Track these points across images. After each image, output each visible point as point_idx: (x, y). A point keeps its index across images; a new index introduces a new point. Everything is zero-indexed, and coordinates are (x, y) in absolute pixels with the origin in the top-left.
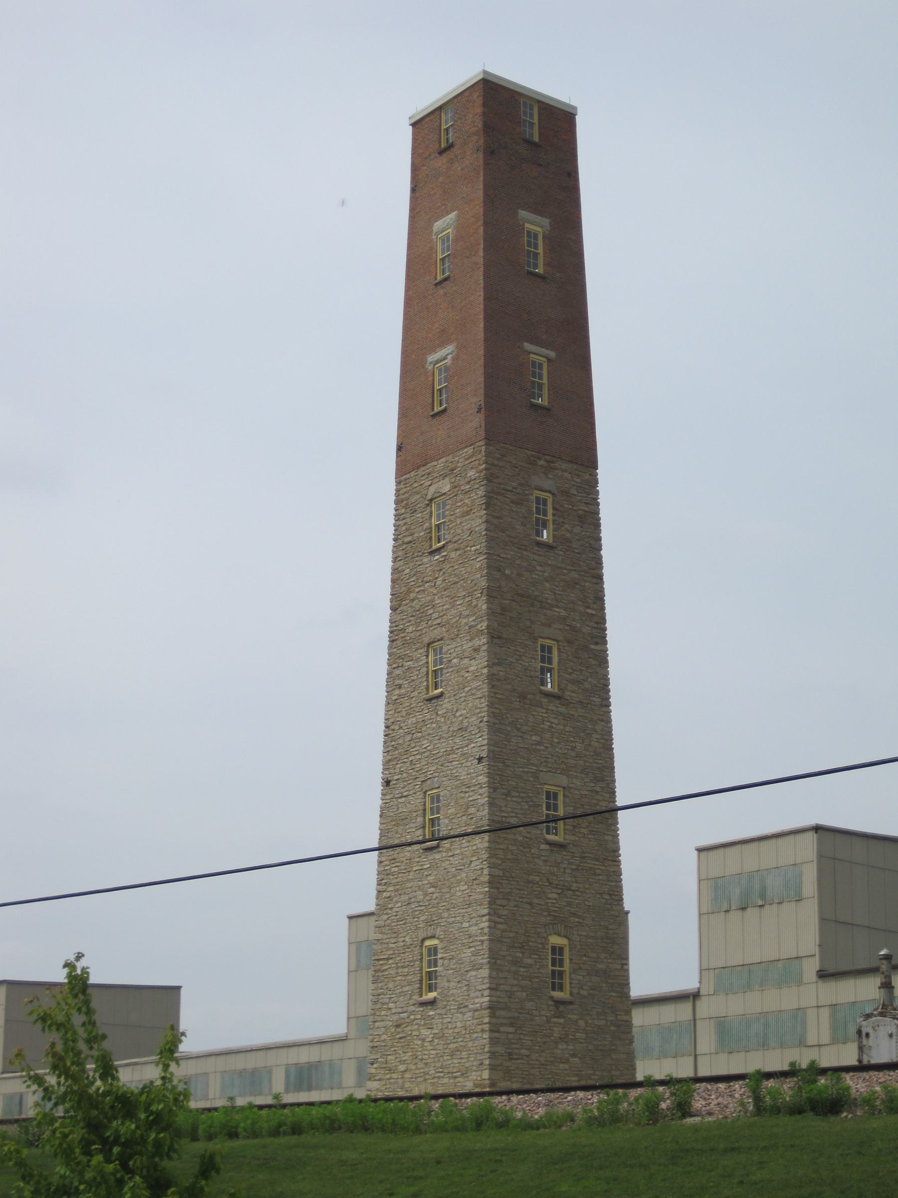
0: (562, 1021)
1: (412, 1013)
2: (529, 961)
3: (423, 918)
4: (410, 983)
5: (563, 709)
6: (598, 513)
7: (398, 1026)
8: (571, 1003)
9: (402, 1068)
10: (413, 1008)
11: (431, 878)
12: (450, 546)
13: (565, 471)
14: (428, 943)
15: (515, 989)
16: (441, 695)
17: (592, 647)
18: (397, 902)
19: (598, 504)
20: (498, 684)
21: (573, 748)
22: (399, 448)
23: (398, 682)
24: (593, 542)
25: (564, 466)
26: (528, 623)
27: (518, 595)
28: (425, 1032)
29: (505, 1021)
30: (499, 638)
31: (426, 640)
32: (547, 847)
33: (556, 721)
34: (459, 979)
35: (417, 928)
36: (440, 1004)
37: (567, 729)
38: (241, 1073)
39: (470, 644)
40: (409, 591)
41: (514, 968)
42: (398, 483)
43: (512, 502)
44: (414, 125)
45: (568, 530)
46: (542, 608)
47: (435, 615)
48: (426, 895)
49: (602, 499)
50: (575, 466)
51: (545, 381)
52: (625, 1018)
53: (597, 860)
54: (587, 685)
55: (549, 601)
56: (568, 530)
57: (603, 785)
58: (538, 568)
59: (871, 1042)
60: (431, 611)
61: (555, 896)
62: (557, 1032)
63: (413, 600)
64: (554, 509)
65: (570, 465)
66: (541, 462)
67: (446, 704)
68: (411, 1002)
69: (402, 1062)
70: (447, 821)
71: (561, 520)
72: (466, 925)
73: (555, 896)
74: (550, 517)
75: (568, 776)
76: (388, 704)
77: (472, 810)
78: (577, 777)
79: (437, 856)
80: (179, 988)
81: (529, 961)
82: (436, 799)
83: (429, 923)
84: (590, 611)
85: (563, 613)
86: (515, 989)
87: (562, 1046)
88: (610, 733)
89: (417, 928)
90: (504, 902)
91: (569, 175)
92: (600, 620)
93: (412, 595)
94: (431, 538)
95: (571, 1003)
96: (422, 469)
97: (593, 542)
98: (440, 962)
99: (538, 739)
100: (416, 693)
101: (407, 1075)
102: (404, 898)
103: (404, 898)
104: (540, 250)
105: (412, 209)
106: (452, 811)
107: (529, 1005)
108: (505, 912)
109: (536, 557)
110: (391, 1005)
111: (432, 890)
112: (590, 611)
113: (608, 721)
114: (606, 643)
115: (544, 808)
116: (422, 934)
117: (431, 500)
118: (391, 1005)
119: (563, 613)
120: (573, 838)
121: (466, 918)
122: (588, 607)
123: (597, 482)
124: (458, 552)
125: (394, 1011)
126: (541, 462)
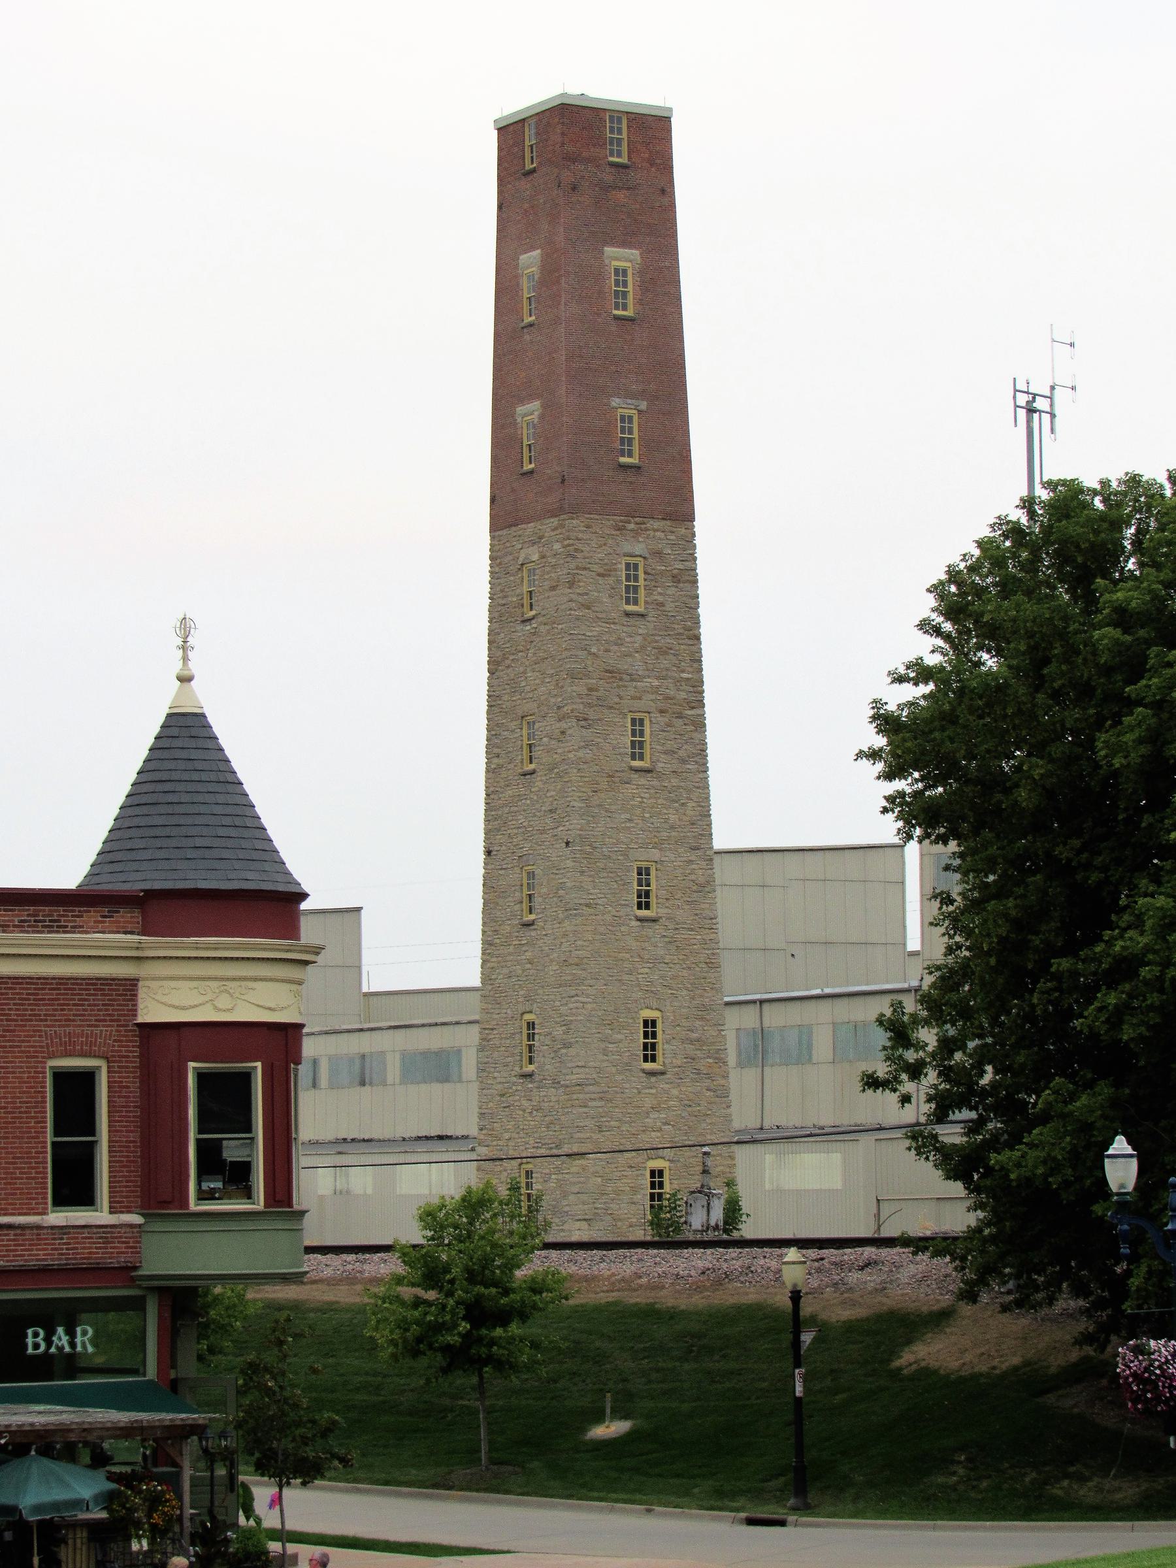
0: (653, 1091)
1: (514, 1084)
2: (619, 1037)
3: (522, 993)
4: (513, 1055)
5: (655, 783)
6: (695, 569)
7: (502, 1095)
8: (663, 1073)
9: (507, 1136)
10: (515, 1079)
11: (529, 954)
12: (541, 619)
13: (657, 530)
14: (527, 1017)
15: (605, 1064)
16: (533, 772)
17: (690, 712)
18: (499, 974)
19: (695, 559)
20: (585, 766)
21: (666, 821)
22: (493, 500)
23: (496, 750)
24: (688, 600)
25: (657, 524)
26: (617, 700)
27: (607, 671)
28: (525, 1103)
29: (593, 1096)
30: (585, 719)
31: (520, 714)
32: (639, 923)
33: (647, 795)
34: (552, 1055)
35: (518, 1002)
36: (537, 1078)
37: (660, 801)
38: (426, 1054)
39: (558, 725)
40: (504, 658)
41: (603, 1045)
42: (492, 538)
43: (599, 575)
44: (499, 130)
45: (660, 594)
46: (632, 680)
47: (528, 688)
48: (524, 971)
49: (699, 553)
50: (668, 523)
51: (636, 435)
52: (722, 1082)
53: (692, 930)
54: (681, 753)
55: (640, 673)
56: (660, 594)
57: (699, 853)
58: (628, 640)
59: (693, 1209)
60: (523, 684)
61: (647, 970)
62: (648, 1102)
63: (508, 667)
64: (645, 573)
65: (663, 523)
66: (632, 526)
67: (538, 782)
68: (513, 1073)
69: (507, 1131)
70: (540, 899)
71: (653, 583)
72: (558, 1003)
73: (647, 970)
74: (641, 582)
75: (660, 850)
76: (487, 771)
77: (561, 892)
78: (670, 849)
79: (533, 934)
80: (358, 910)
81: (619, 1037)
82: (532, 875)
83: (528, 998)
84: (685, 675)
85: (656, 683)
86: (605, 1064)
87: (654, 1115)
88: (708, 798)
89: (518, 1002)
90: (592, 982)
91: (663, 191)
92: (697, 685)
93: (508, 662)
94: (522, 605)
95: (663, 1073)
96: (514, 528)
97: (688, 600)
98: (536, 1037)
99: (628, 816)
100: (512, 766)
101: (511, 1143)
102: (505, 971)
103: (505, 971)
104: (630, 288)
105: (500, 230)
106: (545, 890)
107: (619, 1078)
108: (594, 992)
109: (625, 629)
110: (496, 1074)
111: (529, 966)
112: (685, 675)
113: (704, 786)
114: (703, 706)
115: (635, 883)
116: (521, 1008)
117: (522, 565)
118: (496, 1074)
119: (656, 683)
120: (666, 911)
121: (558, 997)
122: (683, 671)
123: (694, 535)
124: (547, 627)
125: (499, 1080)
126: (632, 526)
